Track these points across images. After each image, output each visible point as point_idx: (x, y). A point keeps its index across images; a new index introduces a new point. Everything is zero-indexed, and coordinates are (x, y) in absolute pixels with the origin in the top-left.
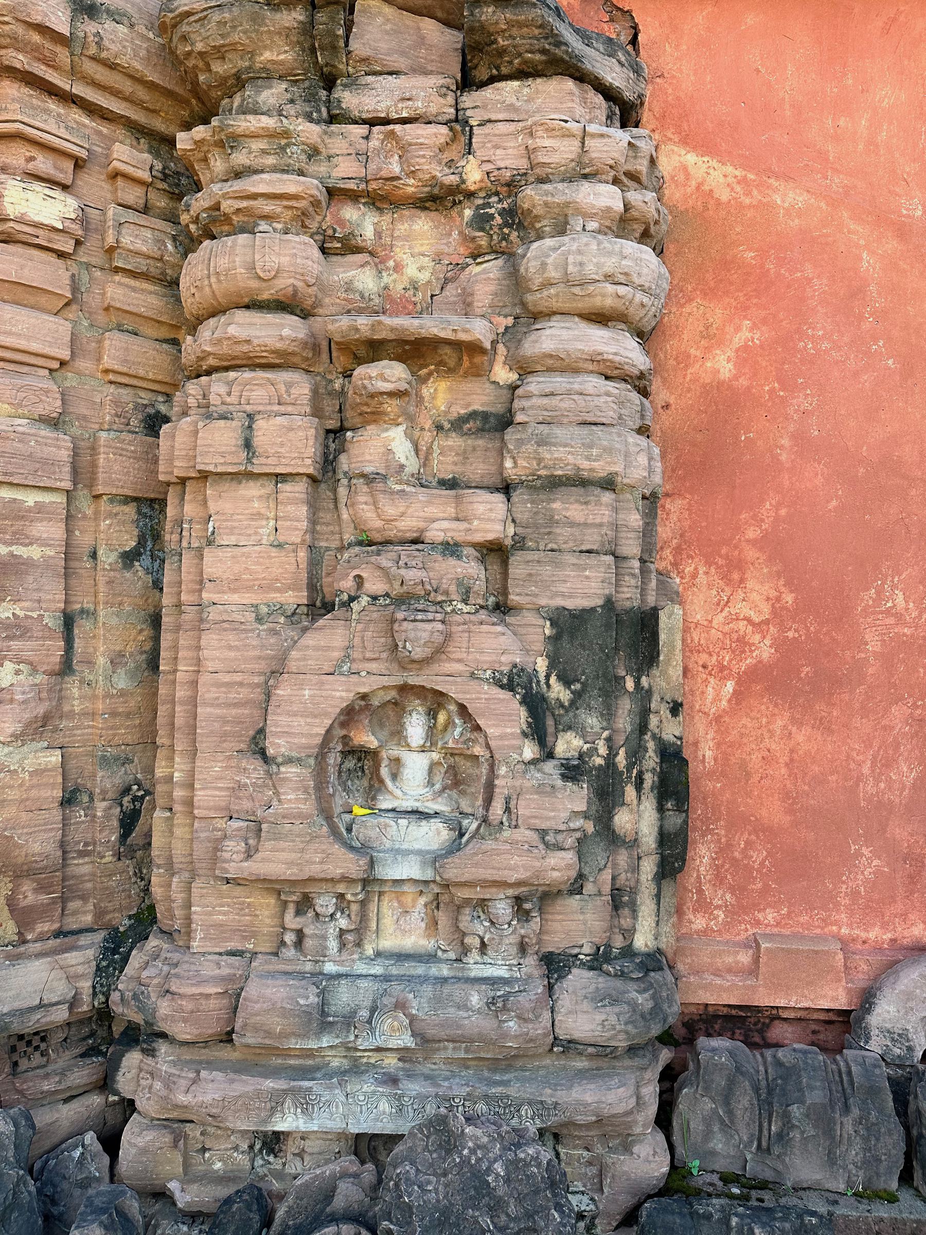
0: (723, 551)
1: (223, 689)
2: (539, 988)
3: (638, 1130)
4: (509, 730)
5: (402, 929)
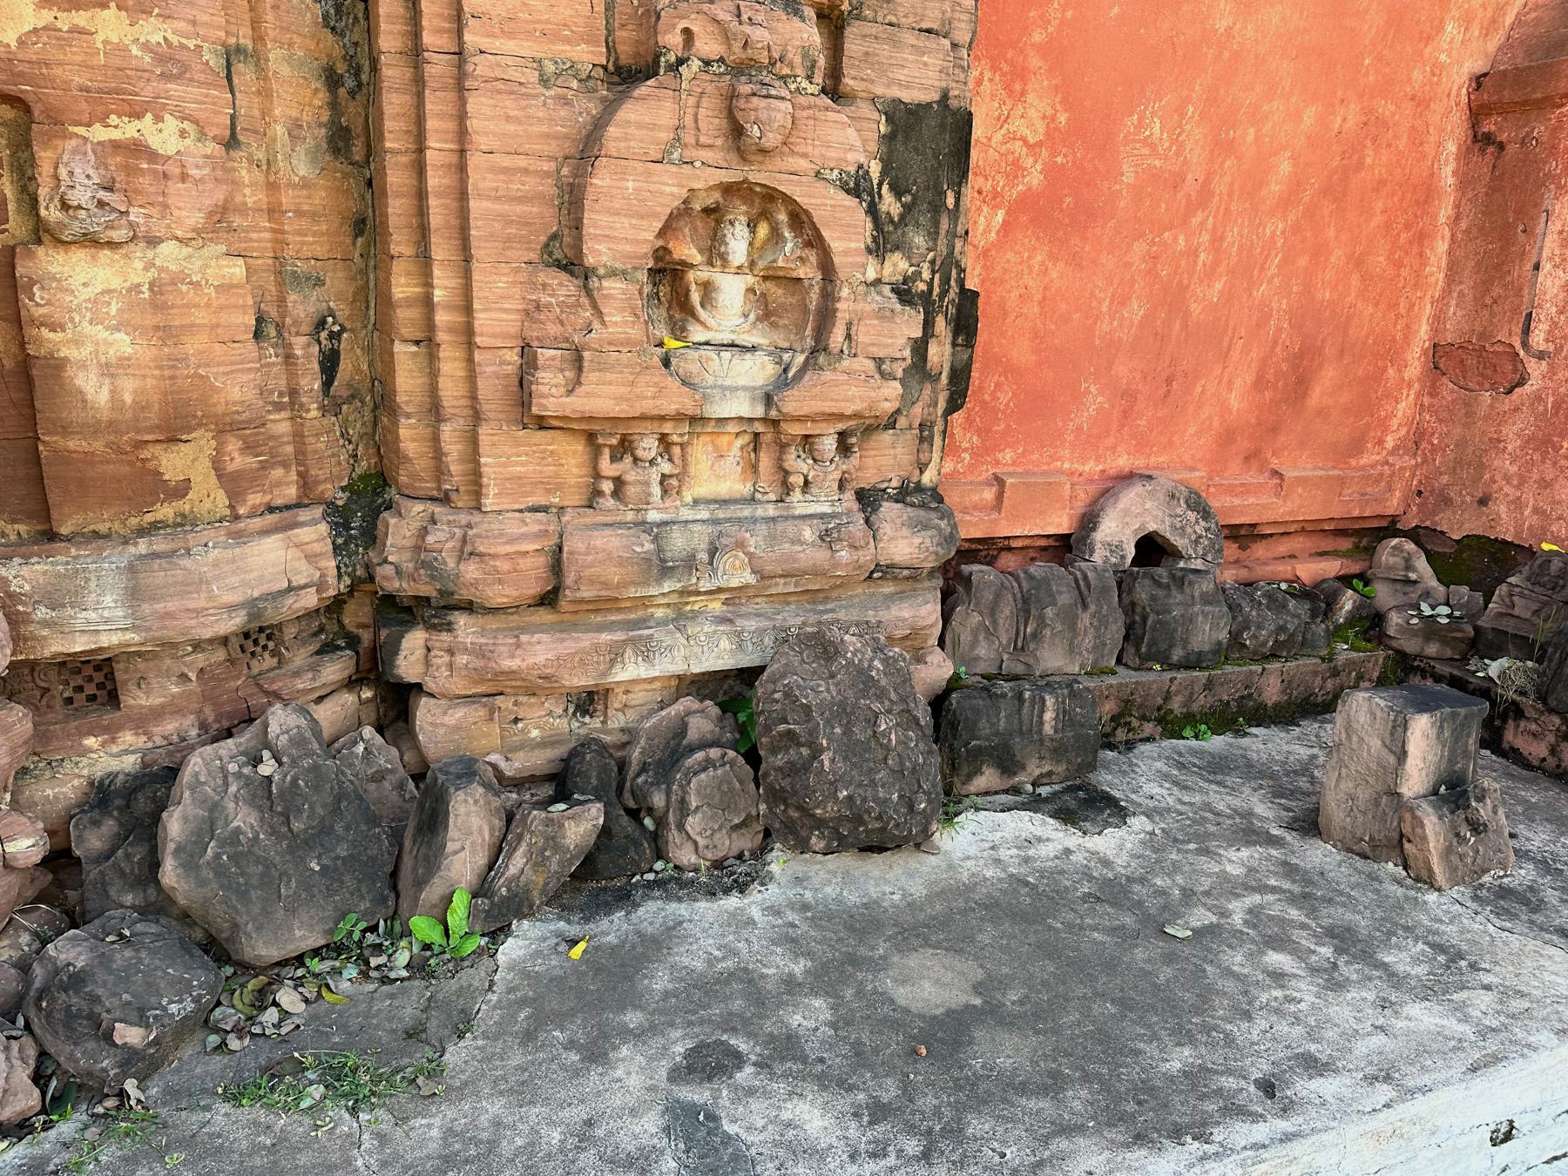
0: (1009, 56)
1: (502, 177)
2: (859, 519)
3: (930, 643)
5: (717, 472)
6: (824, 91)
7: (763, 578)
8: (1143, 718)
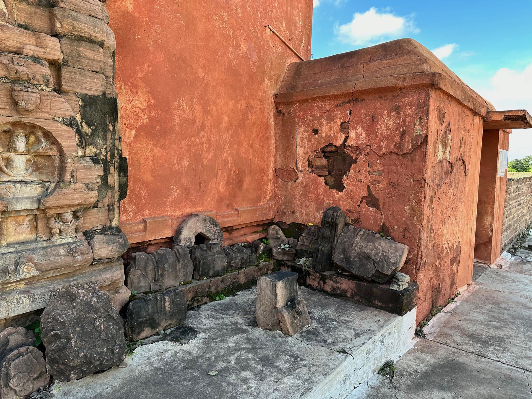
0: (131, 80)
3: (120, 285)
4: (71, 144)
6: (55, 90)
7: (42, 272)
8: (203, 296)
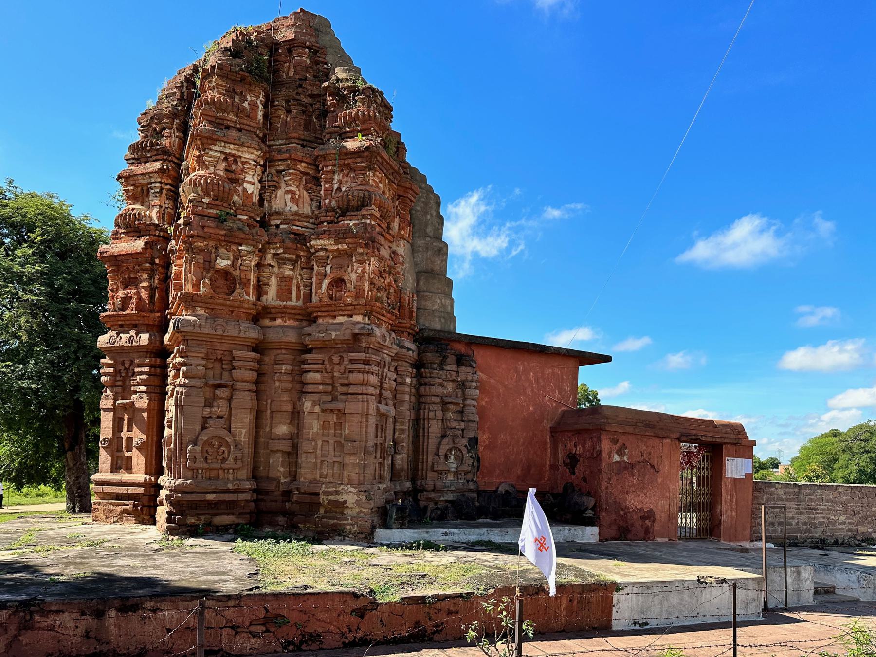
5: (451, 477)
